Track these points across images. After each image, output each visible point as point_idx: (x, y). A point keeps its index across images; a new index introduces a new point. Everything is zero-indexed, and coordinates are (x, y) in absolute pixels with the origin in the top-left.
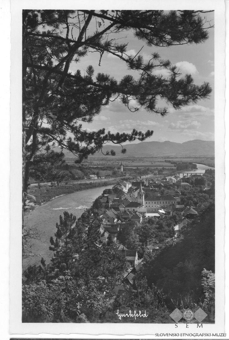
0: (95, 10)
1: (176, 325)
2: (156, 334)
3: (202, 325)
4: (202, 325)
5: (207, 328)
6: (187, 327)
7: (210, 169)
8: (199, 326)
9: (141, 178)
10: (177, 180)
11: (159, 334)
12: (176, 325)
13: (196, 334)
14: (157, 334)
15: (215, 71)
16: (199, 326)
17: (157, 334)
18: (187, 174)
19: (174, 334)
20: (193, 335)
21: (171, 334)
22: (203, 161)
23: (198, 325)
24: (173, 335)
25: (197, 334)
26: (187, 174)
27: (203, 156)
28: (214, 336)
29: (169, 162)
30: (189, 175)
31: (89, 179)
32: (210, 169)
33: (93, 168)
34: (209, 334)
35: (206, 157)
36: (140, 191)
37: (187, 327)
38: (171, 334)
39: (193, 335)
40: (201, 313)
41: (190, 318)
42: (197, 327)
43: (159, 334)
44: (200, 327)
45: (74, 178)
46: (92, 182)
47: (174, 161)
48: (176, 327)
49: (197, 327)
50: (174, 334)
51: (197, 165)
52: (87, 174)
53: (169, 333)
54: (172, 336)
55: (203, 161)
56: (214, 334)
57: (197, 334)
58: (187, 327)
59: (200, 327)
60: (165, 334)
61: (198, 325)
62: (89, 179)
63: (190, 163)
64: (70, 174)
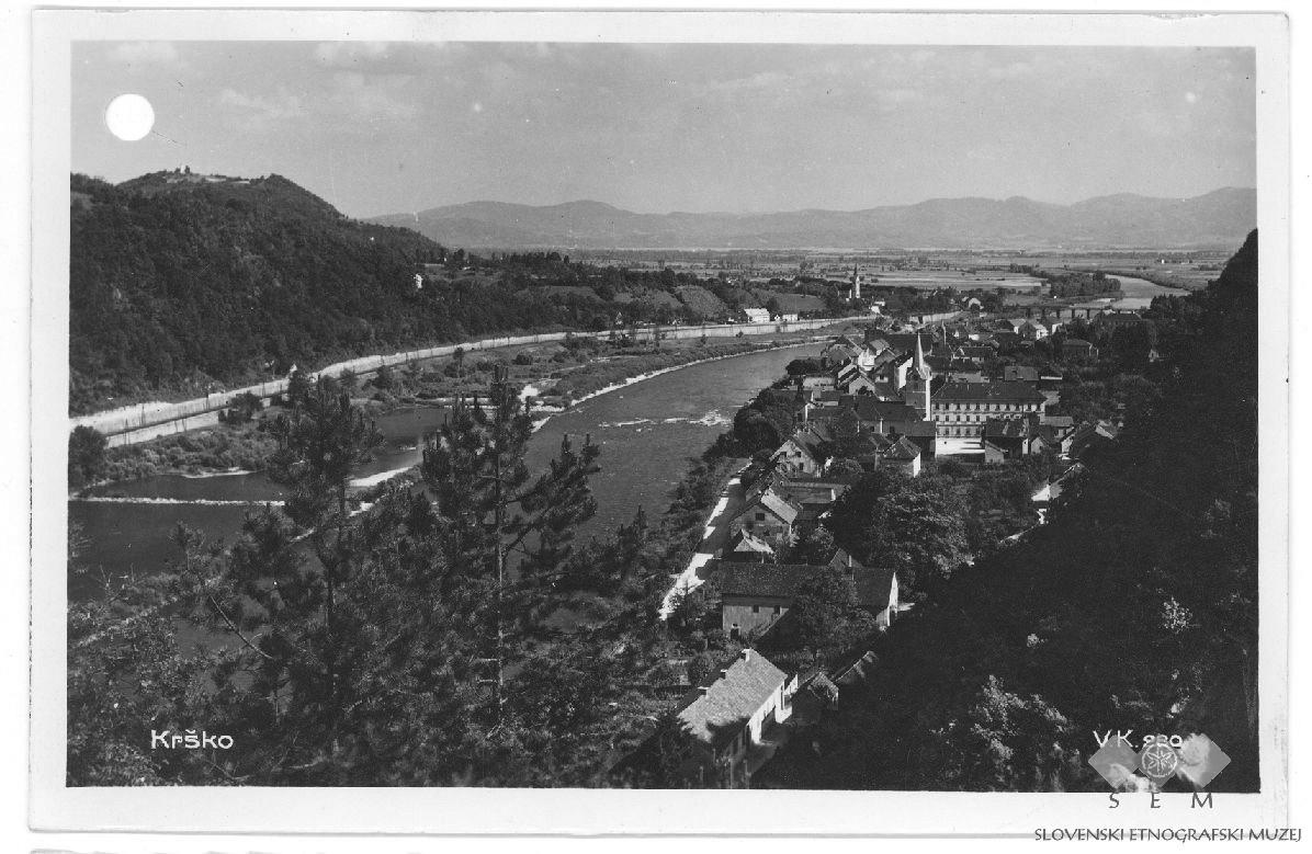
0: (78, 183)
1: (1115, 796)
2: (1039, 832)
3: (1209, 797)
4: (1209, 797)
5: (1230, 807)
6: (1156, 804)
7: (1171, 296)
8: (1199, 802)
9: (921, 322)
10: (1050, 329)
11: (1049, 832)
12: (1112, 799)
13: (1187, 832)
14: (1041, 833)
15: (66, 503)
16: (1199, 802)
17: (1041, 833)
18: (1088, 310)
19: (1107, 833)
20: (1176, 836)
21: (1095, 832)
22: (1145, 268)
23: (1195, 797)
24: (1102, 837)
25: (1192, 832)
26: (1088, 310)
27: (1145, 249)
28: (1257, 838)
29: (1027, 270)
30: (1093, 314)
31: (744, 319)
32: (1171, 296)
33: (759, 285)
34: (1239, 832)
35: (1154, 255)
36: (916, 363)
37: (1156, 804)
38: (1095, 832)
39: (1176, 836)
40: (1197, 753)
41: (1164, 772)
42: (1193, 807)
43: (1049, 832)
44: (1201, 805)
45: (692, 319)
46: (747, 330)
47: (985, 289)
48: (1114, 804)
49: (1193, 807)
50: (1107, 833)
51: (1121, 279)
52: (736, 302)
53: (1084, 825)
54: (1097, 838)
55: (1145, 268)
56: (1257, 832)
57: (1192, 832)
58: (1152, 806)
59: (1201, 805)
60: (1071, 832)
61: (1195, 797)
62: (744, 319)
63: (1099, 275)
64: (675, 304)
